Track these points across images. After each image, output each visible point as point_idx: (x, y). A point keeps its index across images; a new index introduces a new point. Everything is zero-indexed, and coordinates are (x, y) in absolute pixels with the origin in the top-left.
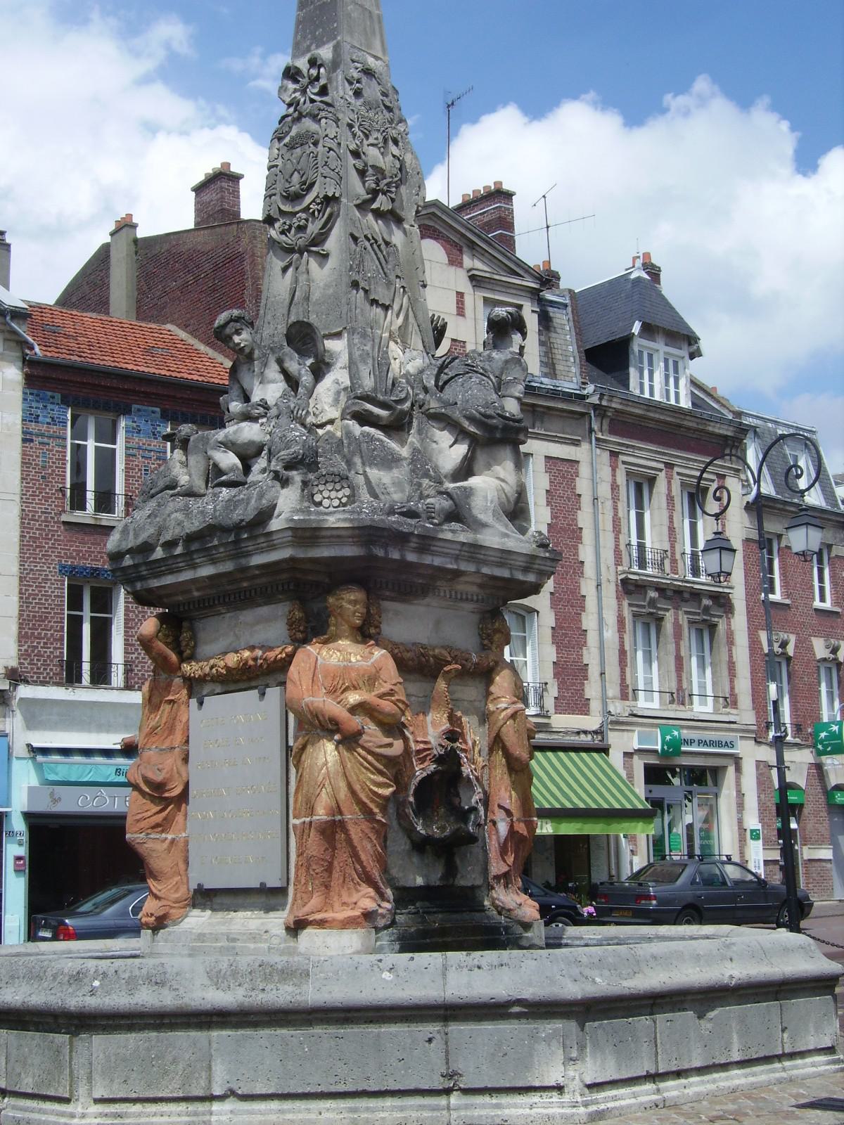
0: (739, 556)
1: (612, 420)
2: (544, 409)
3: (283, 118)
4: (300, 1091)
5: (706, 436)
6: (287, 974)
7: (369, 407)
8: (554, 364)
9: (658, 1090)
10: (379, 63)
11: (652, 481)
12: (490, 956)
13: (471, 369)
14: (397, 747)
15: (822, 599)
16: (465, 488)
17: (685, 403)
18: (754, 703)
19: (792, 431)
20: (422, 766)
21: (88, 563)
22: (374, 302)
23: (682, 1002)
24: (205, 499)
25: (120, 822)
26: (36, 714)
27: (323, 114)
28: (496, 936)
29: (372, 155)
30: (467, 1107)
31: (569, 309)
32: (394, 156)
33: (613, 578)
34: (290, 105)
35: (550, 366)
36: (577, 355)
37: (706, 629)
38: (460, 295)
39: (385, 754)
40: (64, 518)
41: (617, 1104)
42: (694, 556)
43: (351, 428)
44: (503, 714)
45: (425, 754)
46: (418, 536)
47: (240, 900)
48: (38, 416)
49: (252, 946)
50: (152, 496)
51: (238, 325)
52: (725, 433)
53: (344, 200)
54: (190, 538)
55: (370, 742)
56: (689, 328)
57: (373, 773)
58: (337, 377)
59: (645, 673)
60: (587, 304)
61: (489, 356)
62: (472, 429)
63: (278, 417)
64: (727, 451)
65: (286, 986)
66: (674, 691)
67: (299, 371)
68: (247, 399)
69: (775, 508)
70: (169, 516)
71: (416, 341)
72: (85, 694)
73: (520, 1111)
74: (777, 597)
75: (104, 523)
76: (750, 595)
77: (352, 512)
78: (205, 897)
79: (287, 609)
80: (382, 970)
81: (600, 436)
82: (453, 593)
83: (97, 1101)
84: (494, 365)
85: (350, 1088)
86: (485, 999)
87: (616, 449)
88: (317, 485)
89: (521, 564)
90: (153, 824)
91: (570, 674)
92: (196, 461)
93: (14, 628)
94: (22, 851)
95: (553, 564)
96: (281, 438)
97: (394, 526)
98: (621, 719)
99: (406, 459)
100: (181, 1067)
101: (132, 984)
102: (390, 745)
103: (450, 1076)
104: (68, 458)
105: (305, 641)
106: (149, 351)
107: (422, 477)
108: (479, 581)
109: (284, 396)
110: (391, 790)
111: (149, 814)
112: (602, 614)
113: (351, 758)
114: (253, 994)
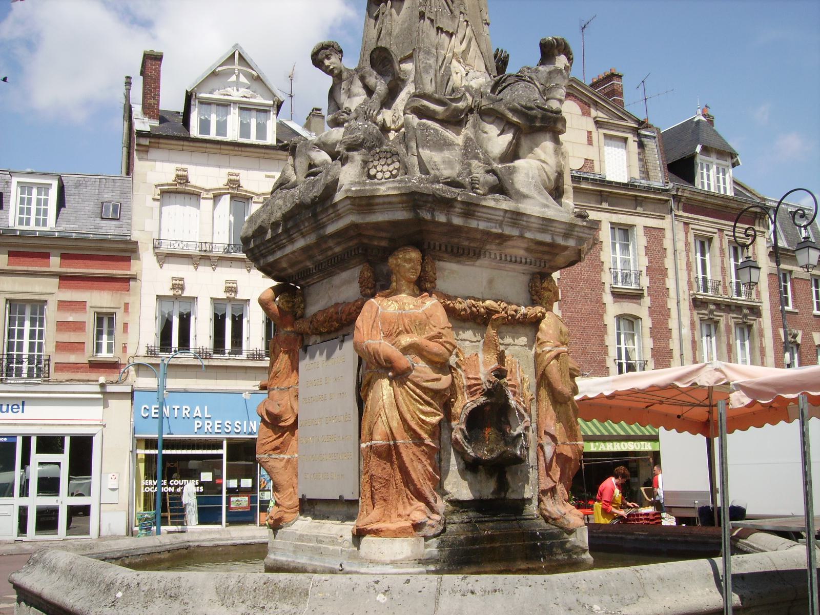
5: (744, 212)
8: (648, 172)
11: (710, 240)
14: (445, 381)
16: (509, 167)
17: (730, 193)
20: (473, 399)
22: (439, 29)
31: (657, 139)
33: (687, 297)
37: (746, 329)
38: (589, 133)
39: (431, 387)
43: (411, 120)
44: (549, 355)
45: (475, 388)
46: (462, 202)
49: (331, 547)
51: (328, 52)
56: (731, 148)
57: (421, 404)
59: (742, 356)
60: (667, 140)
62: (515, 119)
65: (285, 605)
67: (376, 83)
69: (787, 255)
74: (789, 308)
77: (400, 181)
78: (308, 506)
80: (377, 592)
81: (677, 213)
82: (503, 256)
84: (540, 76)
87: (688, 221)
88: (372, 162)
89: (561, 231)
90: (273, 447)
95: (591, 232)
97: (438, 192)
99: (458, 145)
102: (438, 380)
105: (373, 296)
107: (471, 159)
110: (438, 418)
111: (271, 439)
112: (681, 319)
113: (403, 391)
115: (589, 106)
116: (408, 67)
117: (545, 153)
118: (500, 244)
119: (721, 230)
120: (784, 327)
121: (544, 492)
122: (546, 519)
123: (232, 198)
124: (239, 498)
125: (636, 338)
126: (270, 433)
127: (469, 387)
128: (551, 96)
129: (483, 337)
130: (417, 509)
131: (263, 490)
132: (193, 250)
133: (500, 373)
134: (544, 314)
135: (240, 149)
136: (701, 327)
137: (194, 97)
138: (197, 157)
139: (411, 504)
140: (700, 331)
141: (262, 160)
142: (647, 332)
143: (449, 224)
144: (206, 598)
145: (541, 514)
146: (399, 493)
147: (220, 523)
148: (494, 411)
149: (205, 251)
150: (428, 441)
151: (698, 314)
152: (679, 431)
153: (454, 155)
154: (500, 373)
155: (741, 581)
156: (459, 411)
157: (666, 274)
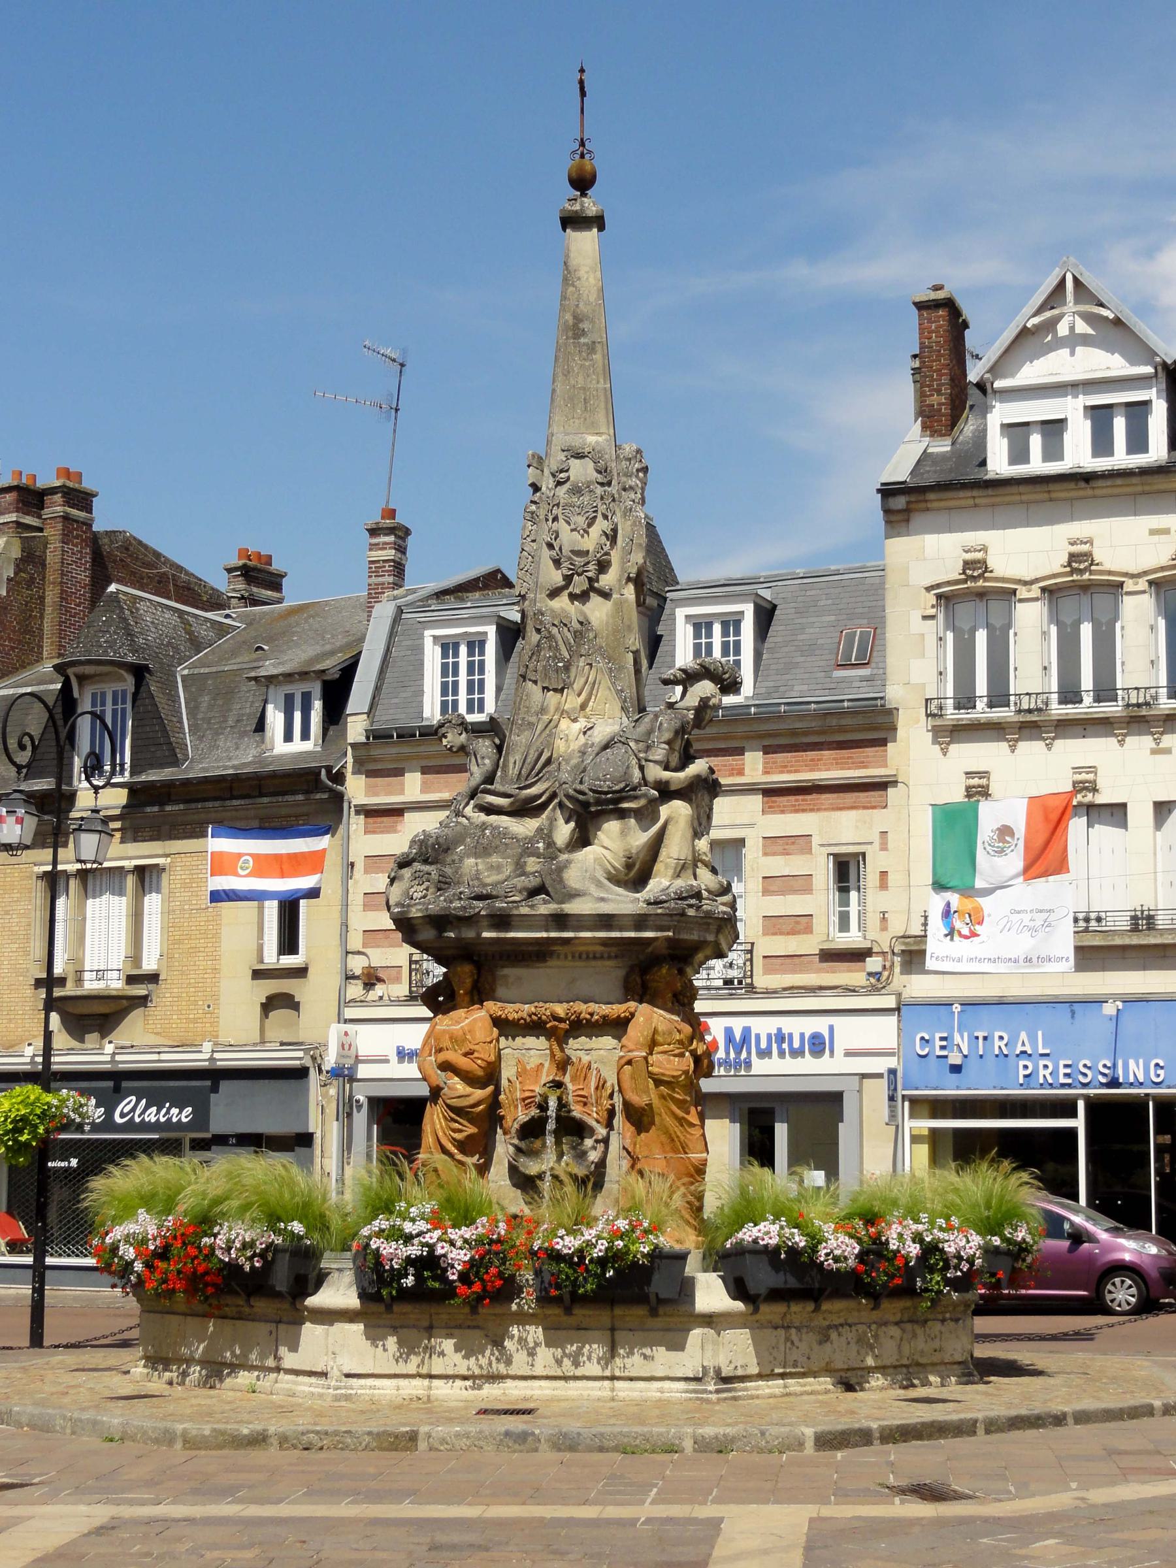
127: (524, 1100)
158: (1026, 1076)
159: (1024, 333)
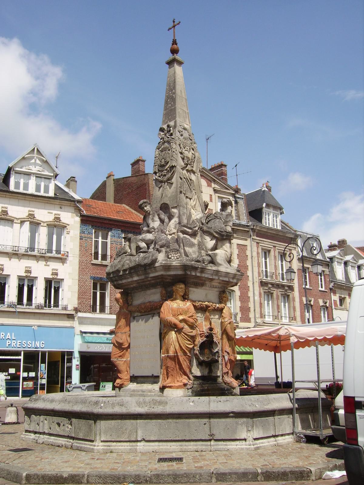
0: (296, 274)
1: (257, 233)
2: (239, 230)
3: (159, 143)
4: (165, 439)
5: (286, 237)
6: (160, 403)
7: (185, 229)
9: (276, 440)
10: (188, 126)
11: (269, 251)
12: (223, 398)
13: (216, 217)
15: (322, 287)
16: (215, 253)
17: (279, 228)
18: (301, 319)
19: (312, 236)
21: (99, 276)
22: (187, 197)
23: (283, 413)
24: (136, 257)
25: (109, 354)
26: (82, 321)
27: (171, 141)
28: (224, 391)
29: (186, 153)
30: (216, 445)
31: (244, 199)
32: (193, 154)
33: (258, 281)
34: (161, 139)
35: (238, 217)
36: (246, 213)
37: (286, 297)
40: (92, 262)
41: (263, 445)
42: (283, 274)
43: (180, 235)
44: (227, 322)
47: (145, 380)
48: (84, 232)
50: (120, 256)
52: (292, 237)
53: (178, 167)
54: (131, 269)
55: (186, 331)
56: (280, 205)
57: (186, 341)
58: (175, 220)
59: (284, 311)
60: (249, 198)
61: (222, 213)
62: (217, 235)
63: (158, 232)
64: (292, 242)
66: (277, 315)
67: (164, 218)
68: (148, 226)
70: (125, 262)
71: (199, 209)
72: (98, 315)
73: (233, 447)
74: (308, 287)
75: (104, 264)
76: (300, 285)
77: (181, 261)
78: (134, 379)
79: (160, 290)
83: (102, 441)
84: (223, 216)
85: (180, 439)
86: (222, 411)
87: (258, 241)
90: (119, 356)
91: (245, 310)
92: (133, 246)
93: (77, 295)
94: (78, 363)
95: (242, 277)
96: (159, 238)
98: (260, 324)
99: (196, 244)
100: (128, 431)
101: (113, 405)
102: (192, 332)
103: (211, 435)
104: (93, 244)
105: (166, 300)
106: (118, 212)
108: (219, 282)
109: (159, 225)
110: (192, 346)
112: (255, 292)
114: (150, 409)
115: (211, 182)
116: (175, 211)
117: (227, 247)
118: (210, 281)
119: (274, 247)
120: (306, 296)
121: (225, 373)
122: (225, 383)
123: (30, 223)
124: (28, 383)
125: (232, 301)
126: (117, 350)
127: (201, 334)
128: (227, 224)
129: (204, 316)
130: (184, 379)
131: (41, 378)
132: (9, 250)
133: (211, 329)
134: (224, 307)
135: (35, 198)
136: (264, 296)
137: (12, 170)
138: (12, 201)
139: (182, 377)
140: (263, 298)
141: (46, 204)
142: (237, 298)
143: (196, 275)
144: (133, 405)
145: (224, 382)
146: (178, 373)
147: (18, 396)
148: (209, 343)
149: (15, 251)
150: (189, 354)
151: (263, 289)
152: (265, 350)
153: (195, 249)
154: (211, 329)
155: (298, 400)
156: (197, 343)
157: (247, 269)
158: (8, 345)
159: (24, 158)
